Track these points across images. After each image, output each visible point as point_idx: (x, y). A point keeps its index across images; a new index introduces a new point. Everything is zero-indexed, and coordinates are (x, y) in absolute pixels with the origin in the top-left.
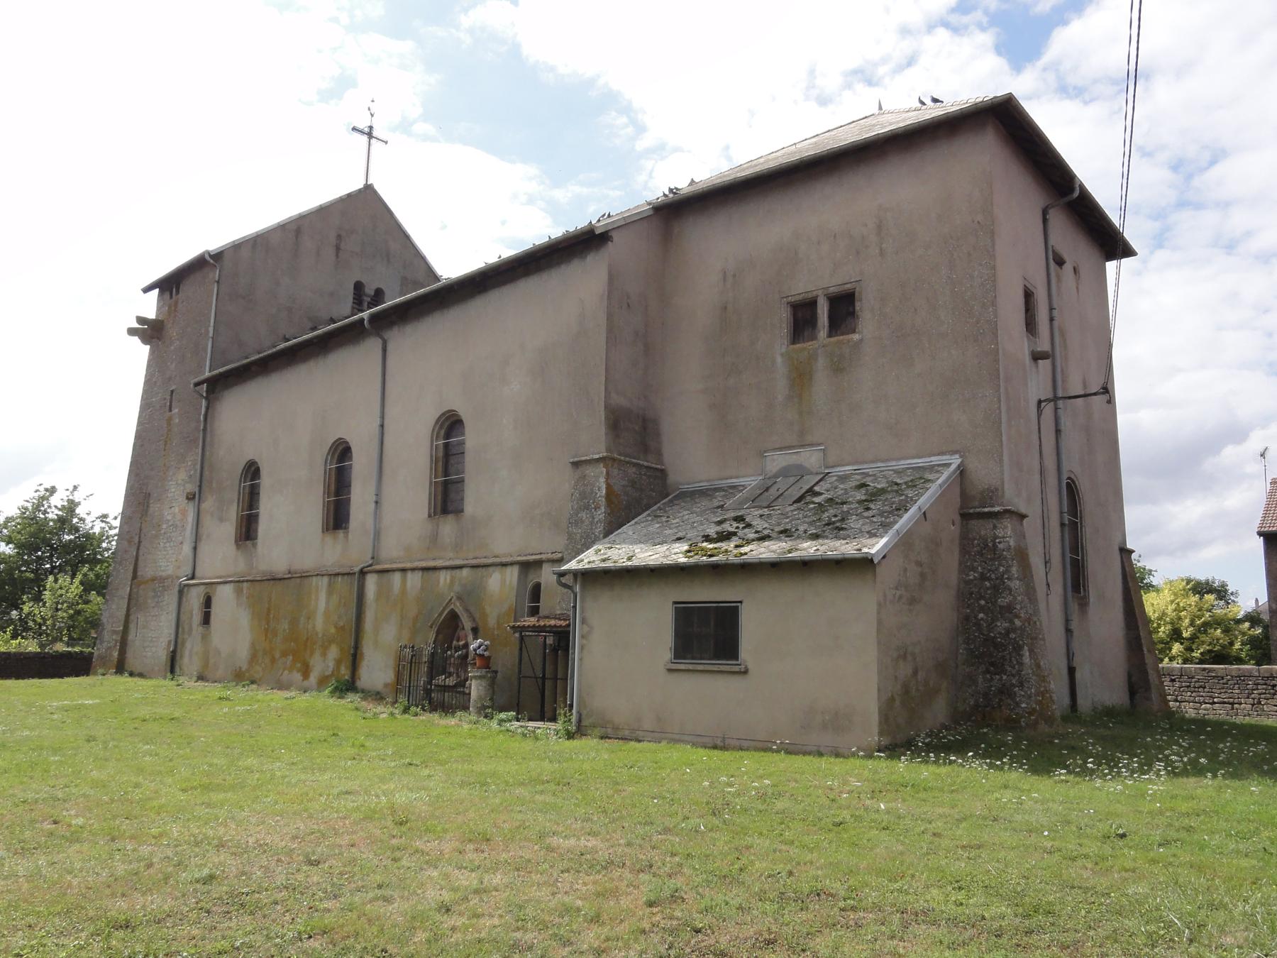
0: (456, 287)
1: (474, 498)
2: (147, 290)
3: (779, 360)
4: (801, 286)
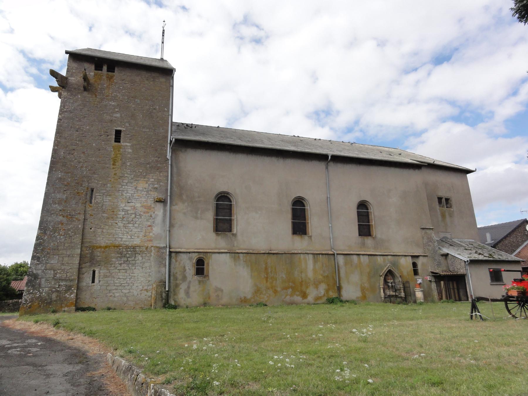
0: (56, 148)
1: (378, 231)
2: (67, 52)
3: (438, 210)
4: (440, 194)
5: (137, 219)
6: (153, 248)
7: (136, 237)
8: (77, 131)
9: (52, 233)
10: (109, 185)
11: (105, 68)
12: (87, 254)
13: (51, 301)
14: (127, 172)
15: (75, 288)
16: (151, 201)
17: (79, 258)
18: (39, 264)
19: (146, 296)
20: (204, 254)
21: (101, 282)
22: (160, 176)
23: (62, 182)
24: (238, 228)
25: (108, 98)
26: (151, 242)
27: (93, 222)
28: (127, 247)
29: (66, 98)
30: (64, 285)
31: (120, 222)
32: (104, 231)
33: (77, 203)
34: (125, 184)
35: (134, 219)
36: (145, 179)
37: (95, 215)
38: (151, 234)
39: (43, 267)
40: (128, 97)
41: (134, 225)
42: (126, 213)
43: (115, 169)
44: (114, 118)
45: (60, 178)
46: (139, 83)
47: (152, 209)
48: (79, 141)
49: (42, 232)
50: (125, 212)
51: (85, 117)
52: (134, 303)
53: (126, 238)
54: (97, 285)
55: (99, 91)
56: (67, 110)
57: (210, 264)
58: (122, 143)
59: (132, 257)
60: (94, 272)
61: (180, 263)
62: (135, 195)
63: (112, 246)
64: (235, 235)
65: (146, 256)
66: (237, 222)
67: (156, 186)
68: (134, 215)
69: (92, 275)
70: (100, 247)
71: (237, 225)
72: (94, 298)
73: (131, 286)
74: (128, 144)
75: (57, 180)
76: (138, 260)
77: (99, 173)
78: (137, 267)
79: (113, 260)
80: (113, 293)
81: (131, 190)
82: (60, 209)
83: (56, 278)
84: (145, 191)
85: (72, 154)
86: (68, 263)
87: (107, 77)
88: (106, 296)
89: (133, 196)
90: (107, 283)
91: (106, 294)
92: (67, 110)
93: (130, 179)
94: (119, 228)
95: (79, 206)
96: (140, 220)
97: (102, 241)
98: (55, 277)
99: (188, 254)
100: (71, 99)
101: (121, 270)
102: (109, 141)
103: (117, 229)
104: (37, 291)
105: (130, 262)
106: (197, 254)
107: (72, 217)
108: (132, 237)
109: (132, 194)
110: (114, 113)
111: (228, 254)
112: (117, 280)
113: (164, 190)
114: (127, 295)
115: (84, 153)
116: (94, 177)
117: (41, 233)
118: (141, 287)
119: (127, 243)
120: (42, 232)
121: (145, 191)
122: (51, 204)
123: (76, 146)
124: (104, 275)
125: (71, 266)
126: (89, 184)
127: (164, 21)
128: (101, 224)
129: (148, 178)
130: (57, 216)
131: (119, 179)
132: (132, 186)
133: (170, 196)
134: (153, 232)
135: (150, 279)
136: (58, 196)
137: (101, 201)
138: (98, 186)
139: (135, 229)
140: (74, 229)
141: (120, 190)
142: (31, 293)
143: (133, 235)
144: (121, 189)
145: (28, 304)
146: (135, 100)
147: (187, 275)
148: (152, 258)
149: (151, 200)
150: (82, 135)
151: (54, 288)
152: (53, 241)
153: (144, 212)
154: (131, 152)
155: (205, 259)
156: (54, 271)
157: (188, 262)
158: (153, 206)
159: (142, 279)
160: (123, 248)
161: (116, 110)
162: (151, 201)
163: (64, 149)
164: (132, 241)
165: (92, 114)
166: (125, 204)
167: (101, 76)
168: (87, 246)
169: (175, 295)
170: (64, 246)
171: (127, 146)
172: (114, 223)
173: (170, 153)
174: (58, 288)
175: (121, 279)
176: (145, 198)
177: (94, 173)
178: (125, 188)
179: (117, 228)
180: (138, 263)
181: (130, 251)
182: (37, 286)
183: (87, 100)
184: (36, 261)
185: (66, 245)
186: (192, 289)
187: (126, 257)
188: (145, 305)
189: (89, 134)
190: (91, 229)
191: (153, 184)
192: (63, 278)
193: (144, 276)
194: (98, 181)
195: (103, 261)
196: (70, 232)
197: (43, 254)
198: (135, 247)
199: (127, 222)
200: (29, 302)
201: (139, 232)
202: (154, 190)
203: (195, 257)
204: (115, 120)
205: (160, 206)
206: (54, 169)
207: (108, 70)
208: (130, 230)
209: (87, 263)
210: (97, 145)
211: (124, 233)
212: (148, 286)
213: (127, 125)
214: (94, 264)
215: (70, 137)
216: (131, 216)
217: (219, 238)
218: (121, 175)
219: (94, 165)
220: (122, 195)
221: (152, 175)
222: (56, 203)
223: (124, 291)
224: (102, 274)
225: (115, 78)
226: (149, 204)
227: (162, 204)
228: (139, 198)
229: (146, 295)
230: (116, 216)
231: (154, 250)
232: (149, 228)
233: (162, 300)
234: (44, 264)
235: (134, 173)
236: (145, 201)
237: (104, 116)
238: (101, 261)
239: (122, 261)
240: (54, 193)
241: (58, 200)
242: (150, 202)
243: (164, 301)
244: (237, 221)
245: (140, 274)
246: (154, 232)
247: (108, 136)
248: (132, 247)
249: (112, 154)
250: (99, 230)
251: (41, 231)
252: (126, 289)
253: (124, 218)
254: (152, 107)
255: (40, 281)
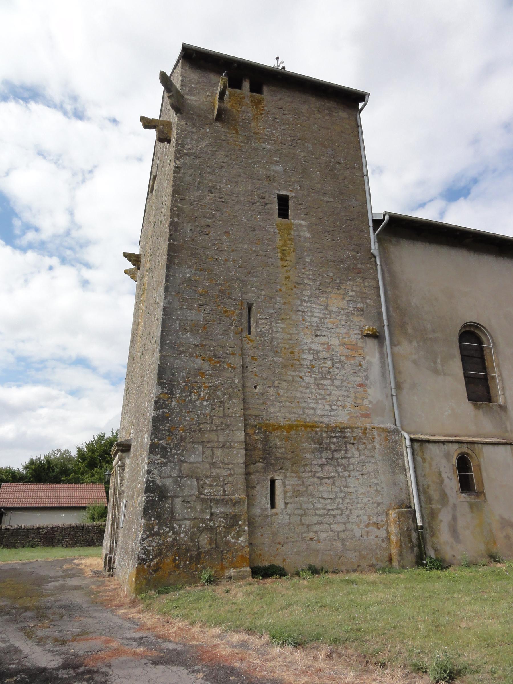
5: (337, 371)
6: (375, 432)
7: (340, 408)
8: (210, 191)
9: (184, 394)
10: (278, 298)
11: (246, 85)
12: (257, 441)
13: (200, 554)
14: (307, 275)
15: (244, 522)
16: (355, 334)
17: (243, 452)
18: (165, 463)
19: (377, 539)
20: (469, 446)
21: (289, 506)
22: (365, 287)
23: (193, 288)
24: (507, 394)
25: (257, 136)
26: (367, 420)
27: (258, 374)
28: (329, 429)
29: (185, 130)
30: (221, 513)
31: (307, 374)
32: (281, 392)
33: (225, 332)
34: (306, 298)
35: (331, 370)
36: (339, 292)
37: (261, 359)
38: (366, 402)
39: (175, 471)
40: (292, 138)
41: (333, 383)
42: (316, 357)
43: (286, 268)
44: (273, 173)
45: (190, 280)
46: (307, 115)
47: (360, 351)
48: (216, 210)
49: (165, 391)
50: (313, 354)
51: (222, 167)
52: (357, 554)
53: (323, 410)
54: (282, 514)
55: (241, 124)
56: (189, 151)
57: (483, 468)
58: (293, 220)
59: (341, 450)
60: (273, 482)
61: (430, 465)
62: (326, 321)
63: (301, 426)
64: (503, 408)
65: (366, 448)
66: (502, 384)
67: (360, 305)
68: (329, 363)
69: (269, 491)
70: (280, 427)
71: (503, 390)
72: (280, 543)
73: (347, 516)
74: (303, 223)
75: (183, 284)
76: (352, 457)
77: (259, 275)
78: (352, 474)
79: (306, 455)
80: (316, 532)
81: (318, 310)
82: (195, 342)
83: (203, 496)
84: (343, 315)
85: (207, 234)
86: (222, 462)
87: (252, 101)
88: (303, 539)
89: (324, 323)
90: (301, 509)
91: (302, 535)
92: (189, 151)
93: (314, 288)
94: (307, 388)
95: (230, 338)
96: (343, 372)
97: (278, 414)
98: (202, 494)
99: (441, 445)
100: (193, 133)
101: (323, 478)
102: (268, 213)
103: (305, 390)
104: (168, 529)
105: (338, 462)
106: (456, 446)
107: (220, 359)
108: (334, 407)
109: (321, 319)
110: (271, 163)
111: (509, 447)
112: (319, 502)
113: (375, 314)
114: (342, 535)
115: (226, 232)
116: (250, 281)
117: (162, 393)
118: (365, 518)
119: (326, 420)
120: (165, 391)
121: (343, 315)
122: (177, 332)
123: (212, 219)
124: (294, 491)
125: (229, 469)
126: (243, 293)
127: (277, 58)
128: (273, 378)
129: (345, 289)
130: (190, 357)
131: (294, 289)
132: (319, 303)
133: (389, 326)
134: (369, 397)
135: (379, 499)
136: (190, 315)
137: (268, 330)
138: (260, 300)
139: (335, 390)
140: (226, 386)
141: (299, 311)
142: (157, 534)
143: (334, 403)
144: (300, 308)
145: (152, 560)
146: (303, 145)
147: (448, 491)
148: (377, 455)
149: (355, 332)
150: (219, 200)
151: (203, 521)
152: (188, 412)
153: (347, 357)
154: (309, 238)
155: (471, 457)
156: (198, 480)
157: (444, 462)
158: (360, 344)
159: (365, 500)
160: (321, 431)
161: (275, 159)
162: (355, 334)
163: (190, 224)
164: (334, 416)
165: (234, 163)
166: (312, 339)
167: (241, 98)
168: (255, 426)
169: (432, 536)
170: (212, 423)
171: (300, 225)
172: (297, 376)
173: (377, 244)
174: (210, 520)
175: (325, 499)
176: (345, 328)
177: (249, 273)
178: (307, 306)
179: (304, 387)
180: (353, 464)
181: (334, 437)
182: (166, 516)
183: (223, 137)
184: (159, 456)
185: (216, 421)
186: (461, 523)
187: (330, 450)
188: (377, 559)
189: (233, 198)
190: (255, 387)
191: (354, 301)
192: (218, 498)
193: (368, 492)
194: (258, 289)
195: (287, 459)
196: (219, 393)
197: (172, 440)
198: (344, 428)
199: (320, 376)
200: (155, 557)
201: (343, 396)
202: (359, 313)
203: (455, 451)
204: (275, 177)
205: (372, 344)
206: (177, 262)
207: (252, 90)
208: (328, 392)
209: (259, 462)
210: (248, 220)
211: (316, 399)
212: (378, 515)
213: (297, 186)
214: (271, 464)
215: (199, 202)
216: (324, 363)
217: (480, 412)
218: (297, 280)
219: (247, 256)
220: (303, 320)
221: (351, 283)
222: (186, 331)
223: (335, 527)
224: (289, 488)
225: (264, 103)
226: (354, 342)
227: (376, 341)
228: (334, 327)
229: (377, 537)
230: (298, 363)
231: (379, 435)
232: (361, 389)
233: (412, 548)
234: (175, 463)
235: (320, 278)
236: (346, 333)
237: (254, 168)
238: (284, 458)
239: (324, 460)
240: (181, 308)
241: (189, 323)
242: (354, 337)
243: (415, 549)
244: (502, 380)
245: (359, 489)
246: (370, 398)
247: (266, 204)
248: (338, 429)
249: (278, 239)
250: (272, 391)
251: (163, 387)
252: (339, 523)
253: (313, 367)
254: (333, 160)
255: (172, 504)
